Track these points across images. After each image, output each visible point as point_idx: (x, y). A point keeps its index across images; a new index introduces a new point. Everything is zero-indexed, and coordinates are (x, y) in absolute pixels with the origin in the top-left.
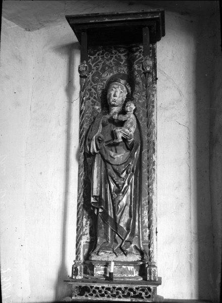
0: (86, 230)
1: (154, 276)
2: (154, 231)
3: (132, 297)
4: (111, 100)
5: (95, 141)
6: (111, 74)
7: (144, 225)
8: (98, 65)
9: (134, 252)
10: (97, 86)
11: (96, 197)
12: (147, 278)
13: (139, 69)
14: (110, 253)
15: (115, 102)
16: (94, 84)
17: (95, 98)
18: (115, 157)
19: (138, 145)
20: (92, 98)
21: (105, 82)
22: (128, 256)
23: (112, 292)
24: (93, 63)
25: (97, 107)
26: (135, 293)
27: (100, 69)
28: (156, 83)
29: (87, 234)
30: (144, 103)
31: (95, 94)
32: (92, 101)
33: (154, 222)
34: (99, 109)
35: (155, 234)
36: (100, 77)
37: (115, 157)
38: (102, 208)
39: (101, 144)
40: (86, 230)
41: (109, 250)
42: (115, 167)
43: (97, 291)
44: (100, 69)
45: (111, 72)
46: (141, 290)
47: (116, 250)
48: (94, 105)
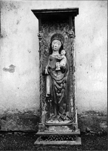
0: (44, 108)
1: (73, 46)
2: (76, 108)
3: (67, 140)
4: (54, 48)
5: (47, 69)
6: (53, 34)
7: (71, 105)
8: (47, 29)
9: (67, 119)
10: (46, 39)
11: (48, 95)
12: (58, 102)
13: (66, 31)
14: (56, 120)
15: (56, 49)
16: (44, 38)
17: (45, 45)
18: (57, 76)
19: (67, 70)
20: (44, 46)
21: (50, 37)
22: (65, 121)
23: (58, 138)
24: (43, 28)
25: (47, 50)
26: (68, 138)
27: (47, 31)
28: (75, 38)
29: (44, 110)
30: (69, 48)
31: (45, 43)
32: (44, 47)
33: (76, 104)
34: (47, 51)
35: (76, 109)
36: (48, 35)
37: (57, 76)
38: (51, 100)
39: (50, 70)
40: (44, 108)
41: (56, 119)
42: (57, 81)
43: (51, 138)
44: (47, 31)
45: (53, 32)
46: (71, 137)
47: (59, 118)
48: (45, 48)
